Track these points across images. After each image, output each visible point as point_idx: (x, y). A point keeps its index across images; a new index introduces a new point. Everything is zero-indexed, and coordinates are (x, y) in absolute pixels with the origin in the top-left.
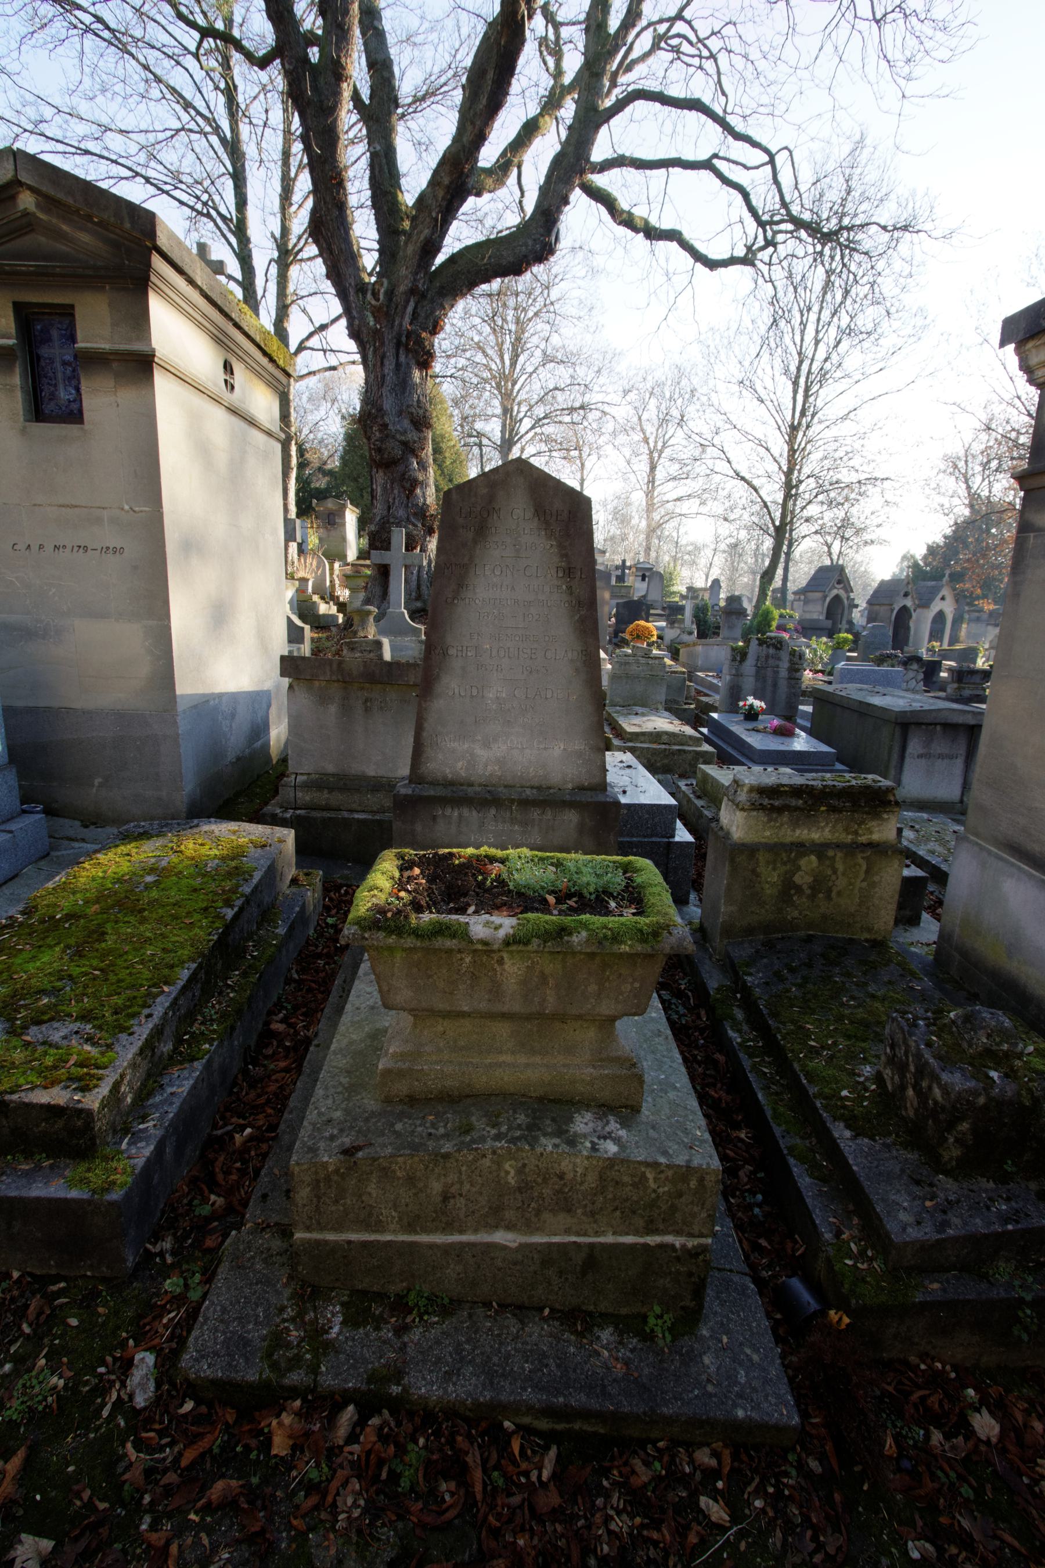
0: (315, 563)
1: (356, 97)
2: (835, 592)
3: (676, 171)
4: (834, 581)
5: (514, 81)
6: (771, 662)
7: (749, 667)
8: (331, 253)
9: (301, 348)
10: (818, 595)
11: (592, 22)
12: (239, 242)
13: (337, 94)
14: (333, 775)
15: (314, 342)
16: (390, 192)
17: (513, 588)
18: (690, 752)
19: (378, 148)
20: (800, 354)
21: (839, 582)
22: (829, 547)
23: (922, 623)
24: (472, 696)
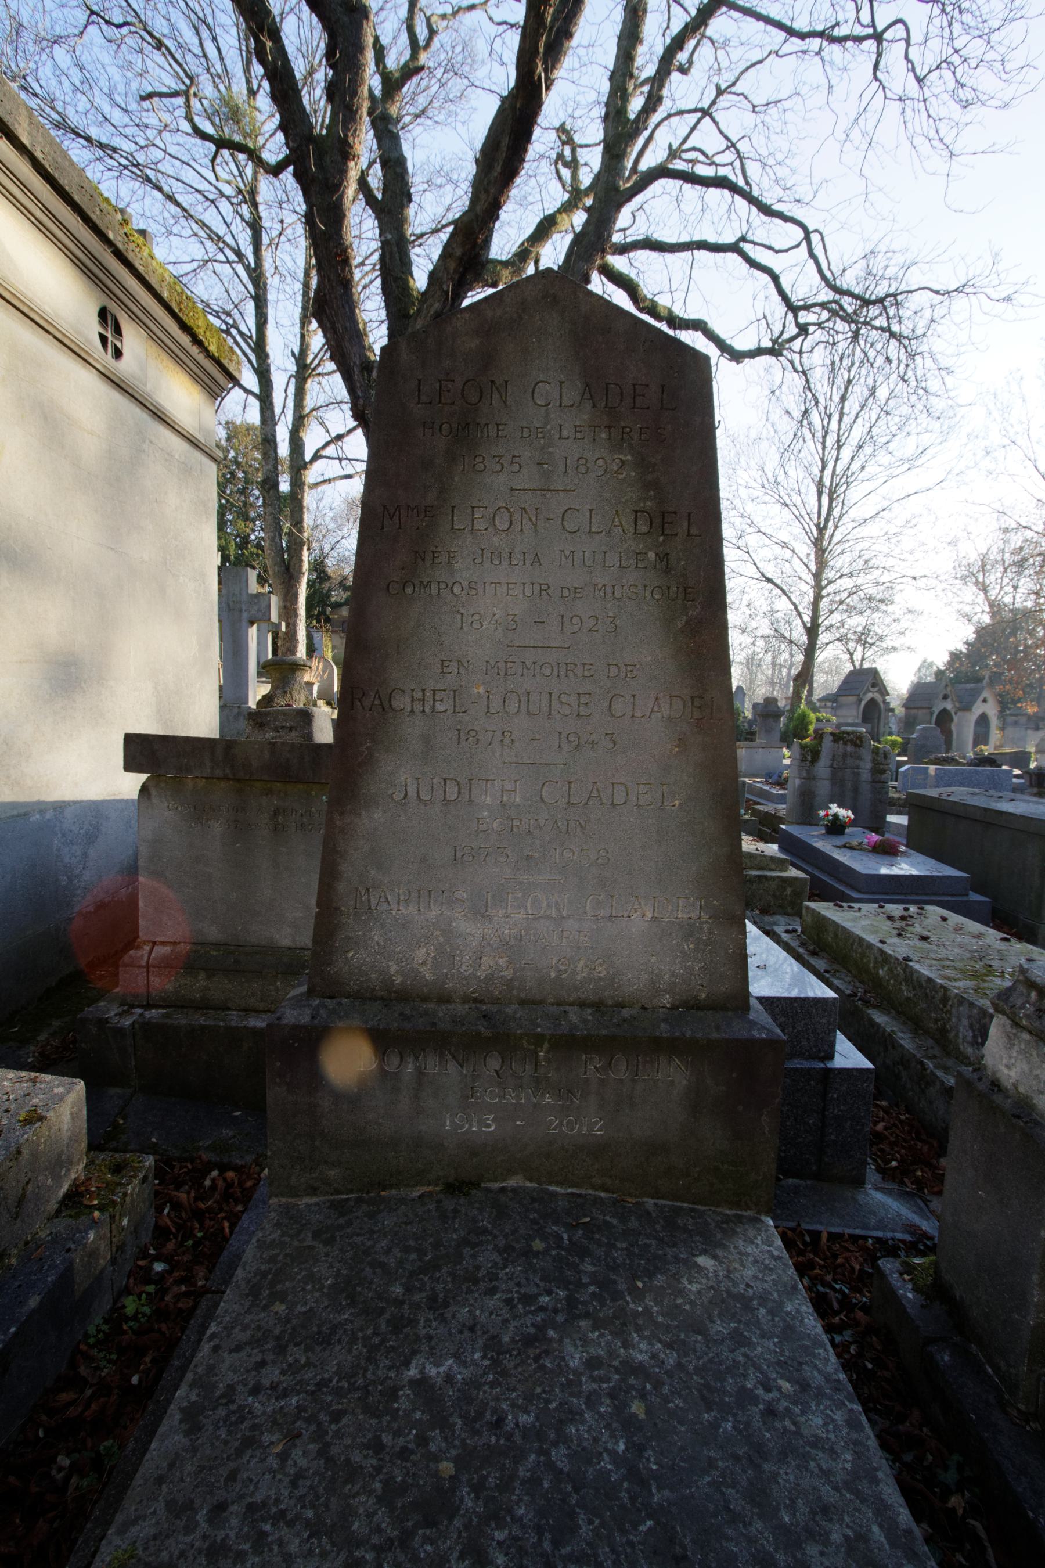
0: (321, 666)
1: (363, 184)
2: (870, 695)
3: (701, 255)
4: (868, 685)
5: (530, 148)
6: (850, 761)
7: (822, 768)
8: (335, 332)
9: (316, 457)
10: (852, 699)
11: (611, 109)
12: (258, 358)
13: (343, 172)
14: (217, 945)
15: (330, 451)
16: (401, 278)
17: (537, 560)
18: (774, 878)
19: (389, 236)
20: (822, 460)
21: (873, 685)
22: (851, 654)
23: (965, 727)
24: (446, 802)
